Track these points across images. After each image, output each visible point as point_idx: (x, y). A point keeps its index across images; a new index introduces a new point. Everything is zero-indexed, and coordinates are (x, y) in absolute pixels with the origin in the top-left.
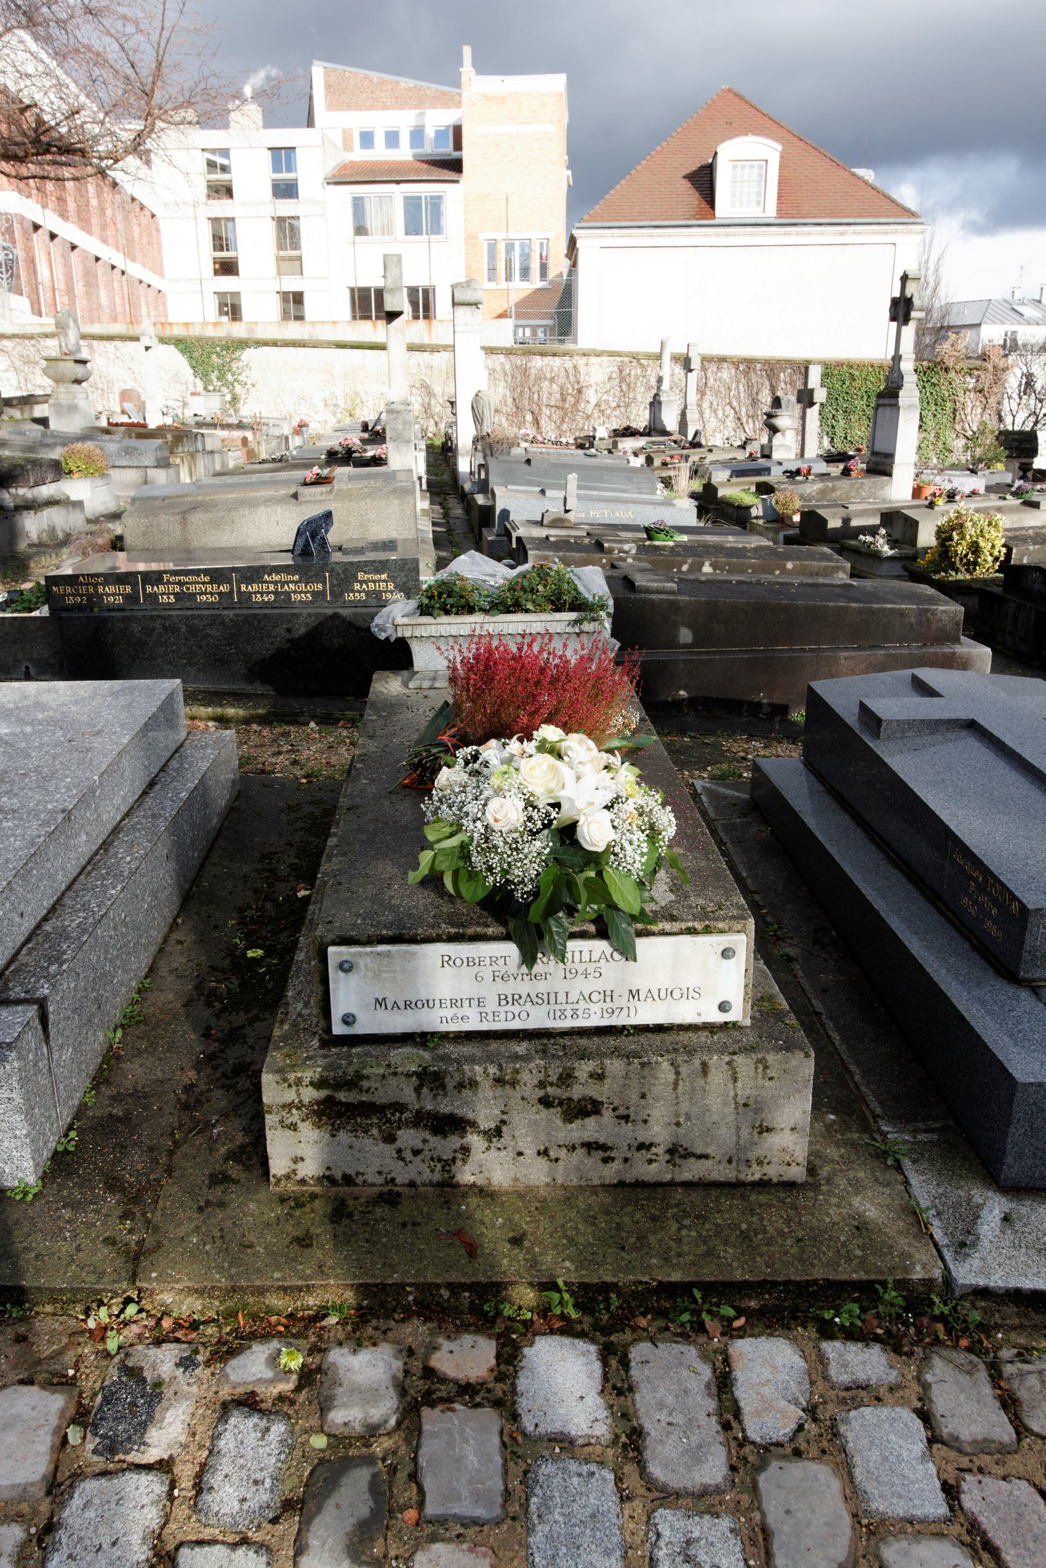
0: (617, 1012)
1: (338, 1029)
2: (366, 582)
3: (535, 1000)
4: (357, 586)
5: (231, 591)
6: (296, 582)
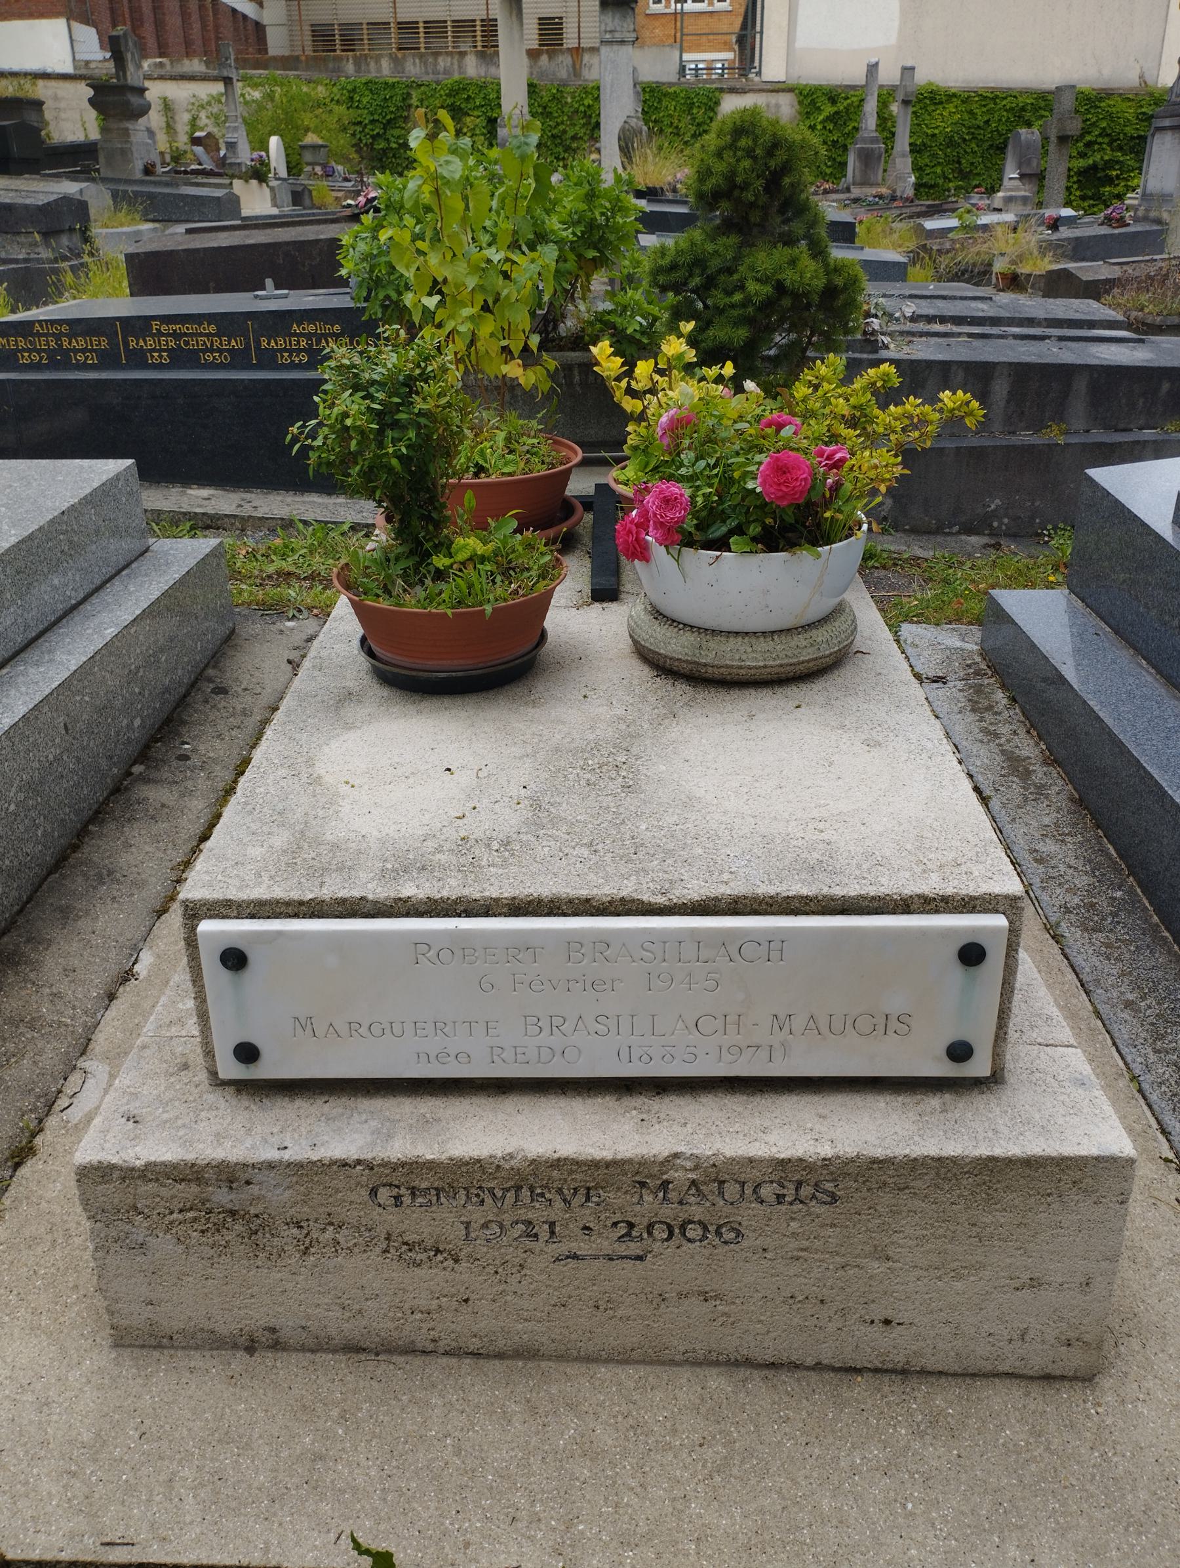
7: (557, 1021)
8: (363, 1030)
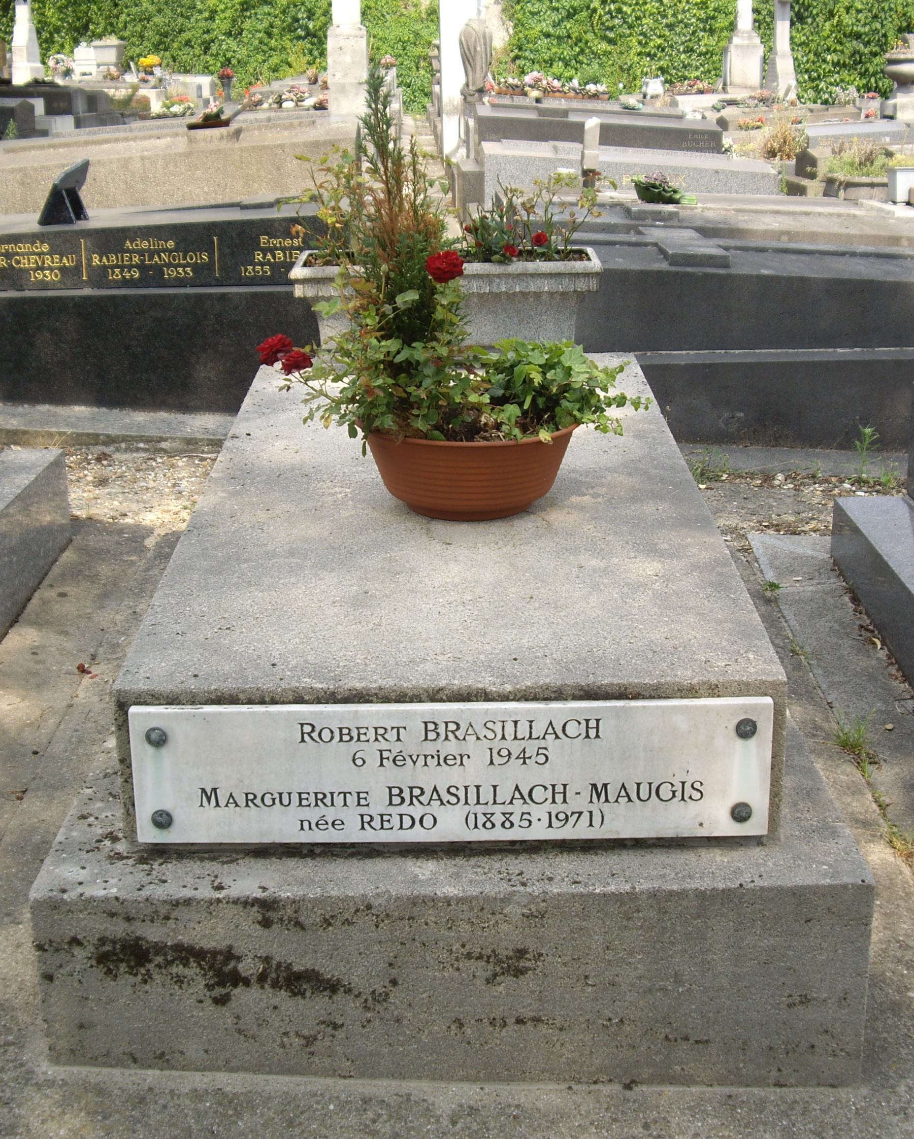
0: (572, 820)
1: (148, 834)
2: (272, 251)
3: (446, 797)
4: (259, 257)
5: (78, 267)
6: (170, 251)
7: (416, 792)
8: (258, 801)
